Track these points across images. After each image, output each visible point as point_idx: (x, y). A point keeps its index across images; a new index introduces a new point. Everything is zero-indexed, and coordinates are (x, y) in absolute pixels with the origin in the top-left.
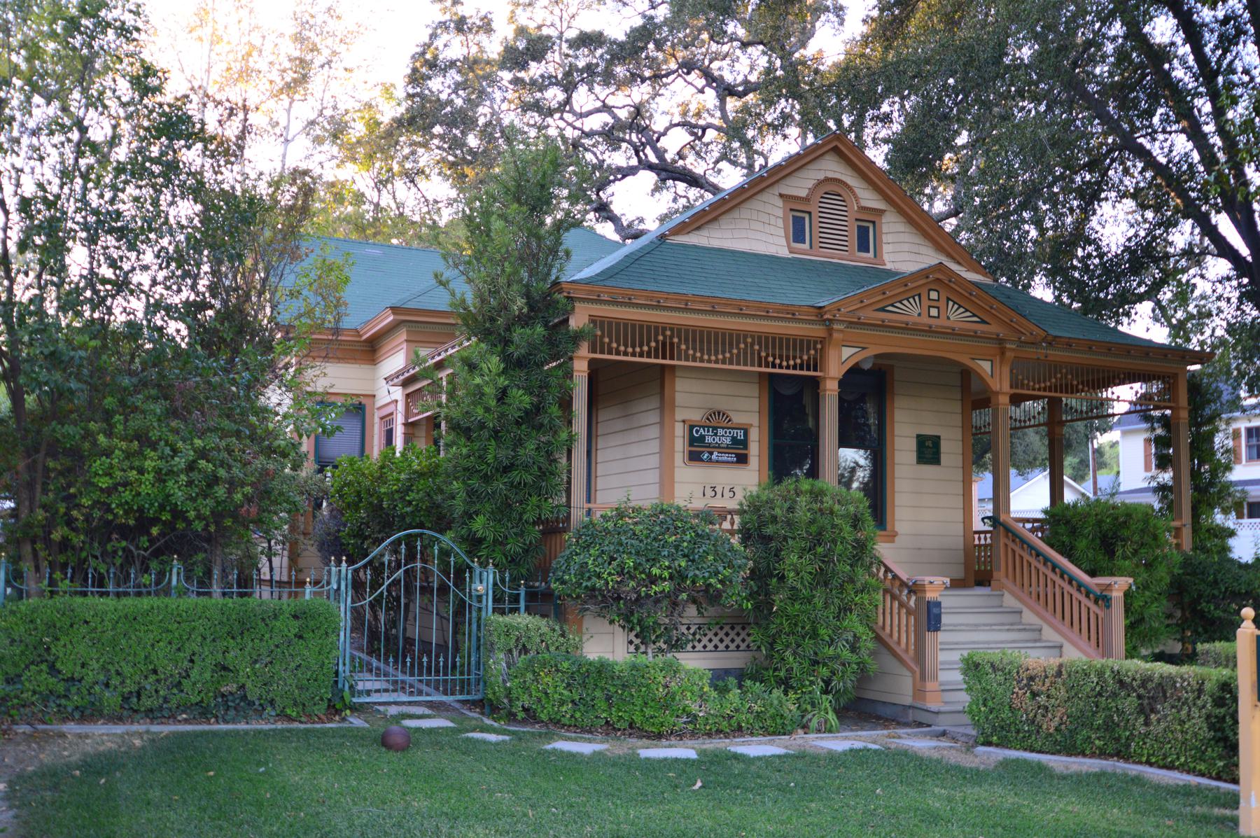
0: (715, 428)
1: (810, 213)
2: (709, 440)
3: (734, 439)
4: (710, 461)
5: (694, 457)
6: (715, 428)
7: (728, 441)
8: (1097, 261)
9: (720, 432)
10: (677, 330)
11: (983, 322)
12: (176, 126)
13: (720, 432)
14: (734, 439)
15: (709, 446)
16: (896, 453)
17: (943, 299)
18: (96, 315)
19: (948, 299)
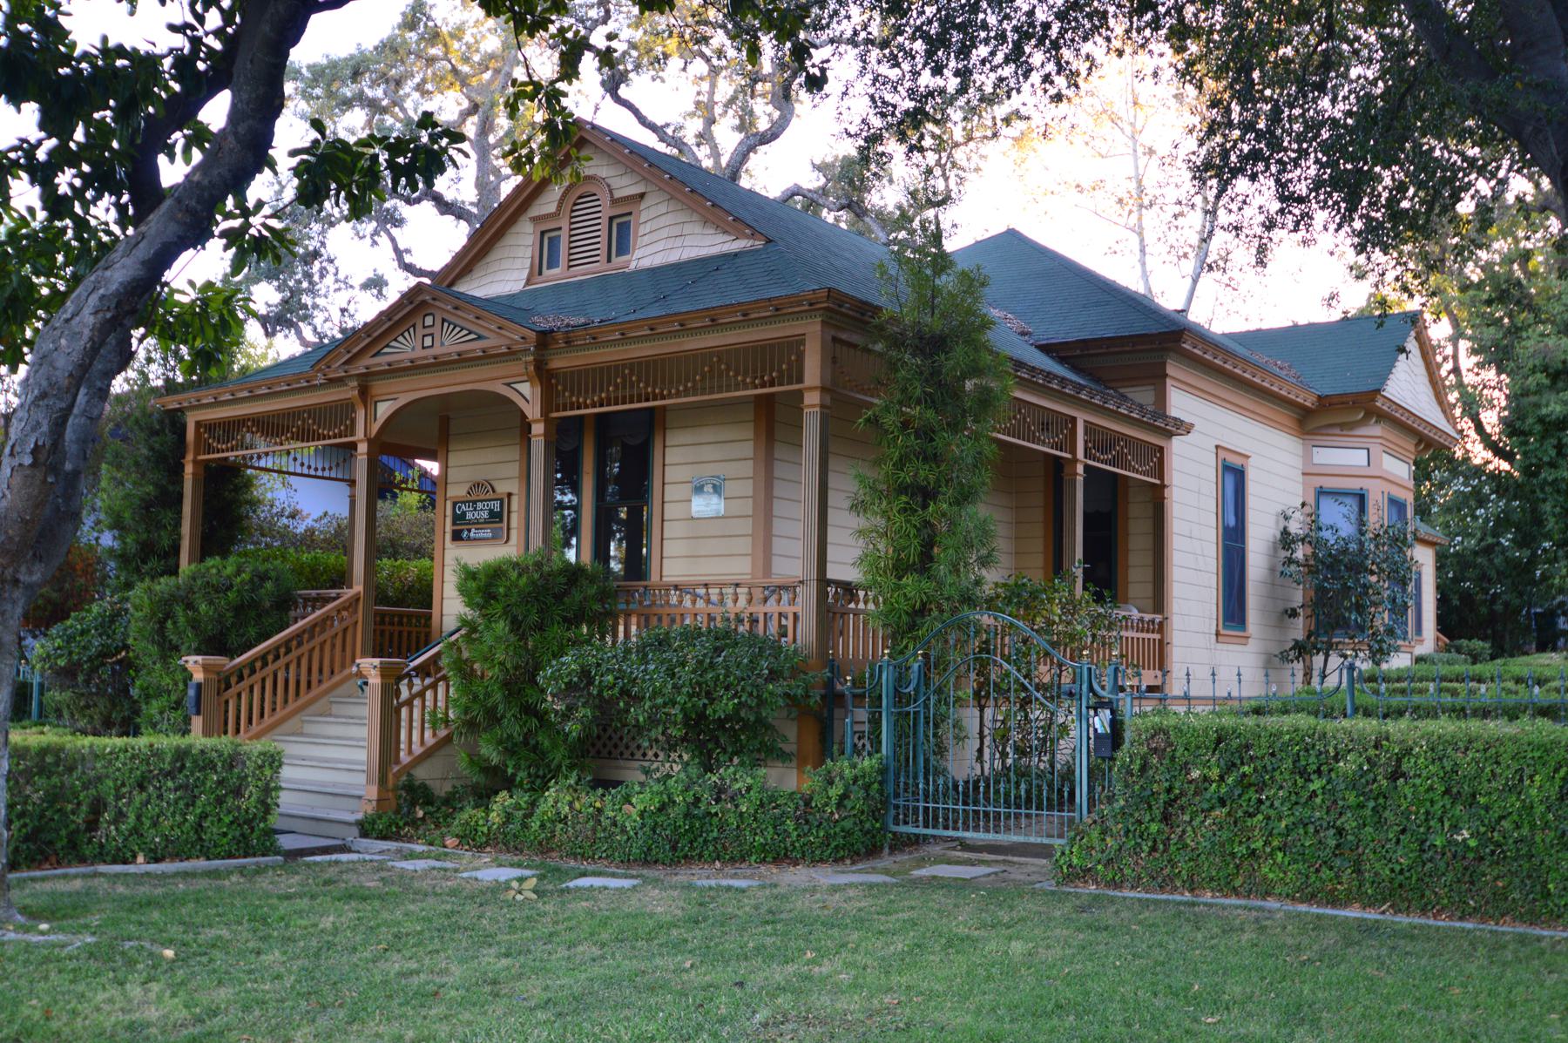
0: (475, 502)
1: (611, 219)
2: (469, 516)
3: (491, 512)
4: (469, 538)
5: (457, 536)
6: (475, 502)
7: (485, 515)
8: (1335, 195)
9: (480, 505)
10: (311, 411)
11: (480, 337)
12: (434, 36)
13: (480, 505)
14: (491, 512)
15: (470, 523)
16: (1131, 522)
17: (438, 322)
18: (1271, 876)
19: (444, 320)
